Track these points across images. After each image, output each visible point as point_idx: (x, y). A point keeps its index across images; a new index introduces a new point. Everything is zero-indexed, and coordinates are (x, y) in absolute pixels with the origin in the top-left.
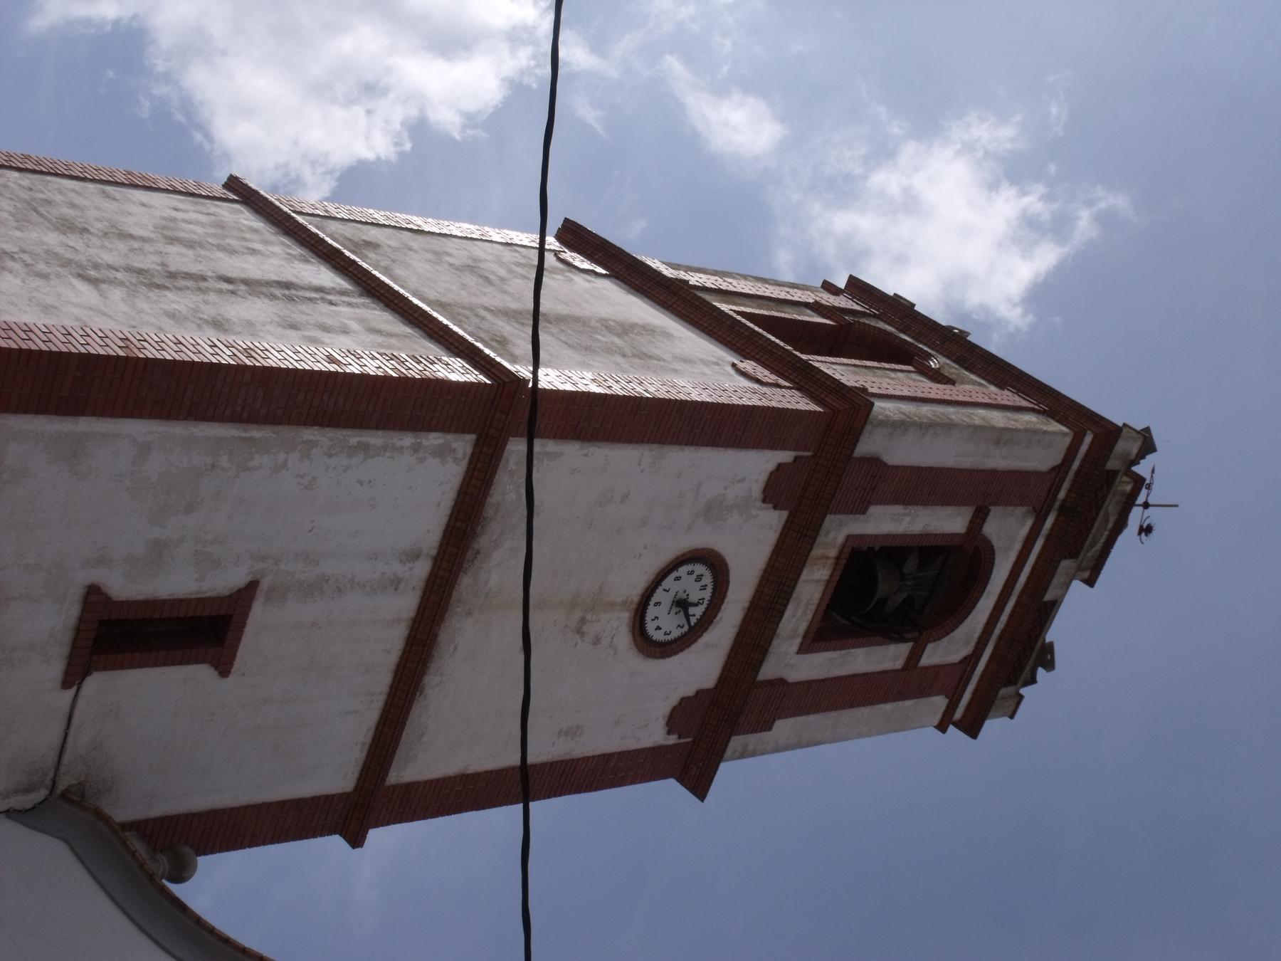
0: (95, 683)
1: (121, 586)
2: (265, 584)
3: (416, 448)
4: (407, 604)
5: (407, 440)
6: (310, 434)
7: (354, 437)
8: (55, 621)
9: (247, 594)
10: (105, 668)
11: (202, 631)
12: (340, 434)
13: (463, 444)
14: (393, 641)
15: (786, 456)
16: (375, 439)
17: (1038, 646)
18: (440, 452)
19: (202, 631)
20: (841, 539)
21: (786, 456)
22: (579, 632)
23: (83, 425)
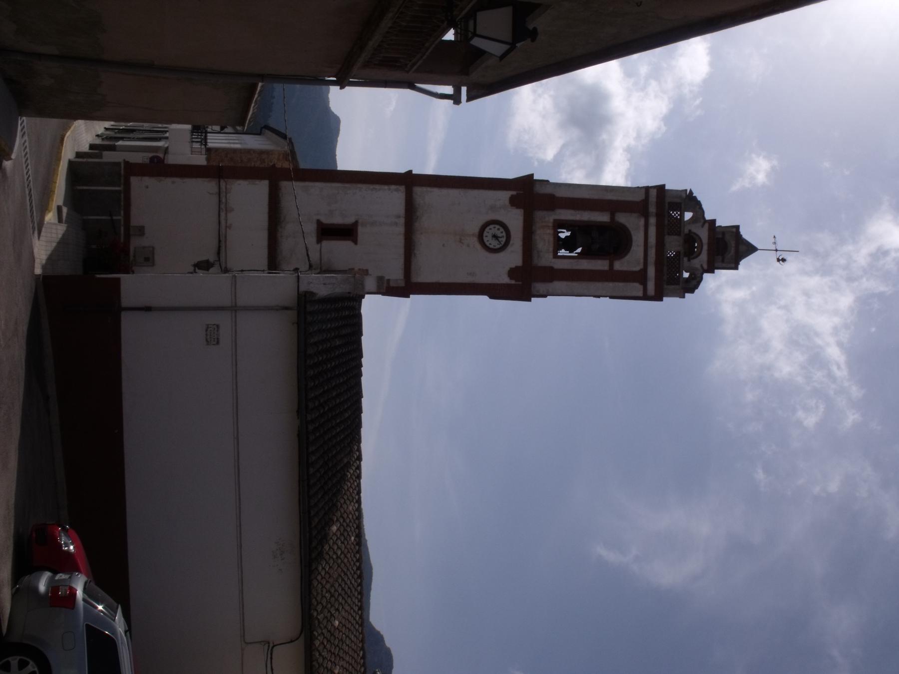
0: (325, 243)
1: (325, 220)
2: (360, 221)
3: (389, 189)
4: (401, 229)
5: (386, 187)
6: (360, 185)
7: (372, 187)
8: (310, 228)
9: (356, 224)
10: (327, 239)
11: (347, 232)
12: (367, 185)
13: (266, 183)
14: (400, 241)
15: (514, 193)
16: (377, 187)
17: (77, 160)
18: (396, 190)
19: (347, 232)
20: (551, 220)
21: (514, 193)
22: (460, 241)
23: (307, 184)
